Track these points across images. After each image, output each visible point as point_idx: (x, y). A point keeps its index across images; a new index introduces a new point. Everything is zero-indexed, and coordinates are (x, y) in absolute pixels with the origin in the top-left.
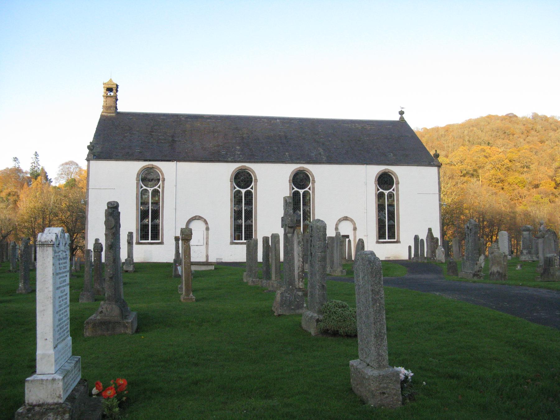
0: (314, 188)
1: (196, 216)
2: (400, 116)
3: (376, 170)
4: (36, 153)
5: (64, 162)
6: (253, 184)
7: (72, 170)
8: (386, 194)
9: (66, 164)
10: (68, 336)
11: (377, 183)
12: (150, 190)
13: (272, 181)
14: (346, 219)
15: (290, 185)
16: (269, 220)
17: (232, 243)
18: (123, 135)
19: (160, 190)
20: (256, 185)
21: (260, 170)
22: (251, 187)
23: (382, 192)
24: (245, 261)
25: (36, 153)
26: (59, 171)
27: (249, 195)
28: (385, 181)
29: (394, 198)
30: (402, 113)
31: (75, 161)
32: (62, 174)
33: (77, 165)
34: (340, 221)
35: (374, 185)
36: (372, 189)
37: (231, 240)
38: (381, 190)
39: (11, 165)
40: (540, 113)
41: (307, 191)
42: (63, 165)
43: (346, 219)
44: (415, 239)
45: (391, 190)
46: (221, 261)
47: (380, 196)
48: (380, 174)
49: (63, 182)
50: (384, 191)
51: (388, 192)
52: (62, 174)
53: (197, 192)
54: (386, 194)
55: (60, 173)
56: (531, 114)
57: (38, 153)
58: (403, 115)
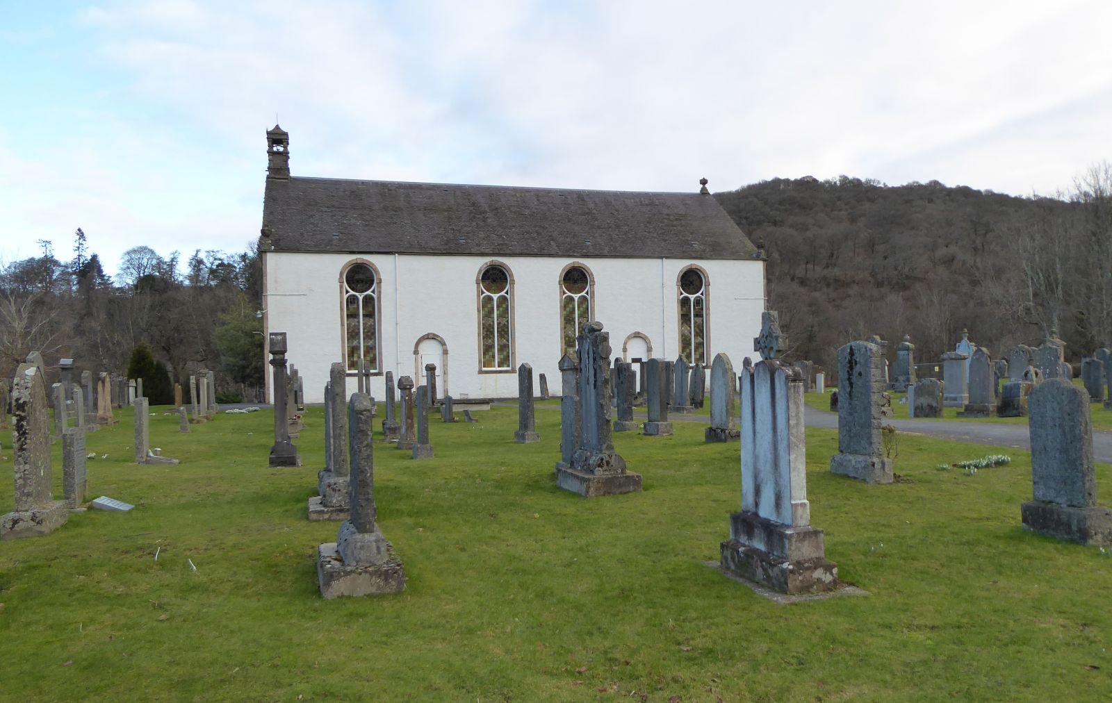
0: (593, 293)
1: (428, 334)
2: (701, 186)
3: (677, 267)
4: (79, 230)
5: (130, 248)
6: (375, 285)
7: (145, 261)
8: (692, 300)
9: (134, 251)
10: (703, 425)
11: (680, 284)
12: (361, 297)
13: (536, 280)
14: (637, 335)
15: (561, 288)
16: (540, 342)
17: (481, 372)
18: (302, 211)
19: (375, 296)
20: (512, 287)
21: (518, 267)
22: (701, 292)
23: (354, 295)
24: (534, 396)
25: (79, 230)
26: (124, 263)
27: (369, 301)
28: (691, 280)
29: (702, 306)
30: (704, 182)
31: (151, 247)
32: (128, 268)
33: (152, 252)
34: (629, 338)
35: (676, 288)
36: (673, 293)
37: (480, 368)
38: (685, 294)
39: (38, 254)
40: (850, 177)
41: (370, 295)
42: (128, 253)
43: (637, 335)
44: (744, 362)
45: (699, 294)
46: (466, 397)
47: (684, 303)
48: (568, 268)
49: (130, 280)
50: (690, 296)
51: (695, 296)
52: (128, 268)
53: (429, 299)
54: (692, 300)
55: (125, 266)
56: (838, 178)
57: (83, 230)
58: (706, 185)
